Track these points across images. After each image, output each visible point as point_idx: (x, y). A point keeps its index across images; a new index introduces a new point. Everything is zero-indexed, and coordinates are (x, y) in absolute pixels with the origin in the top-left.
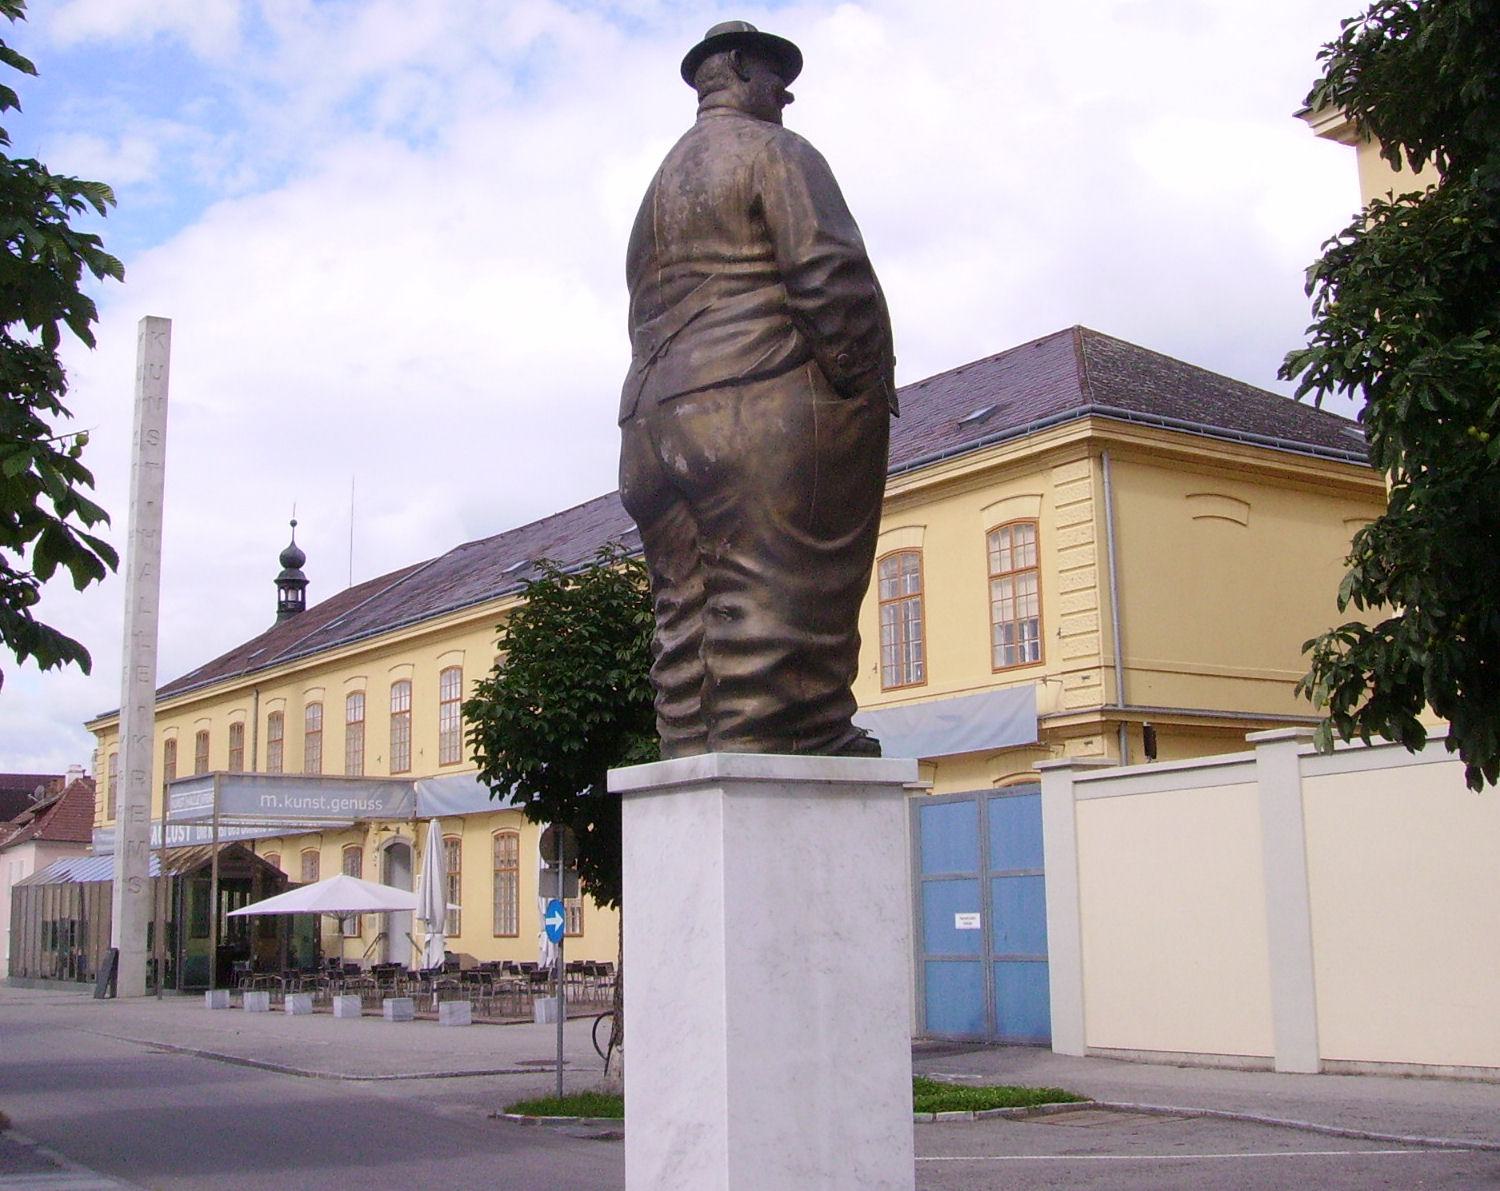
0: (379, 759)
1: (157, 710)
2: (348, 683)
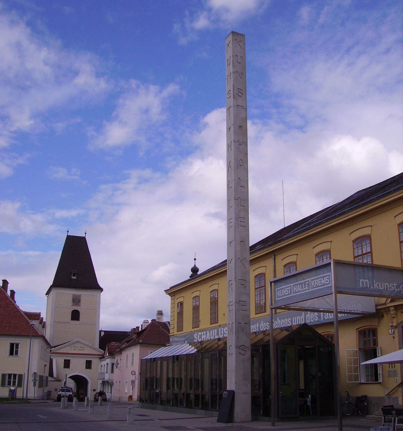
0: (224, 315)
1: (251, 259)
2: (255, 271)
